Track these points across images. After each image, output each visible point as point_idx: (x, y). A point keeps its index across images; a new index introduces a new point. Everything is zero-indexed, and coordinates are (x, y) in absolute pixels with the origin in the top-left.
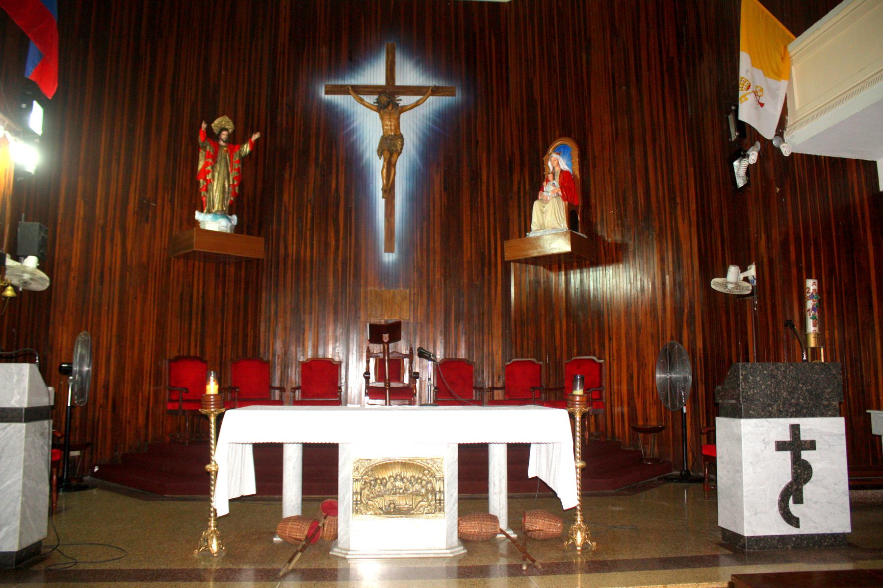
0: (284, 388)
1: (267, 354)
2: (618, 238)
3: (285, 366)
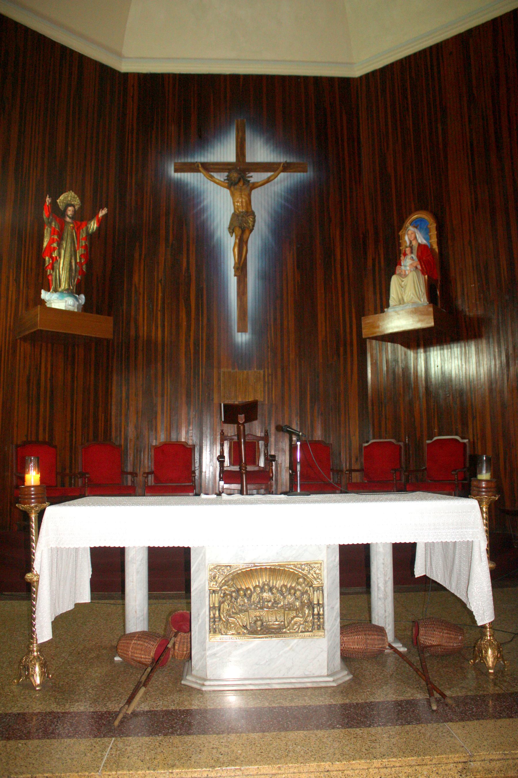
0: (136, 474)
1: (118, 438)
2: (480, 312)
3: (137, 450)
